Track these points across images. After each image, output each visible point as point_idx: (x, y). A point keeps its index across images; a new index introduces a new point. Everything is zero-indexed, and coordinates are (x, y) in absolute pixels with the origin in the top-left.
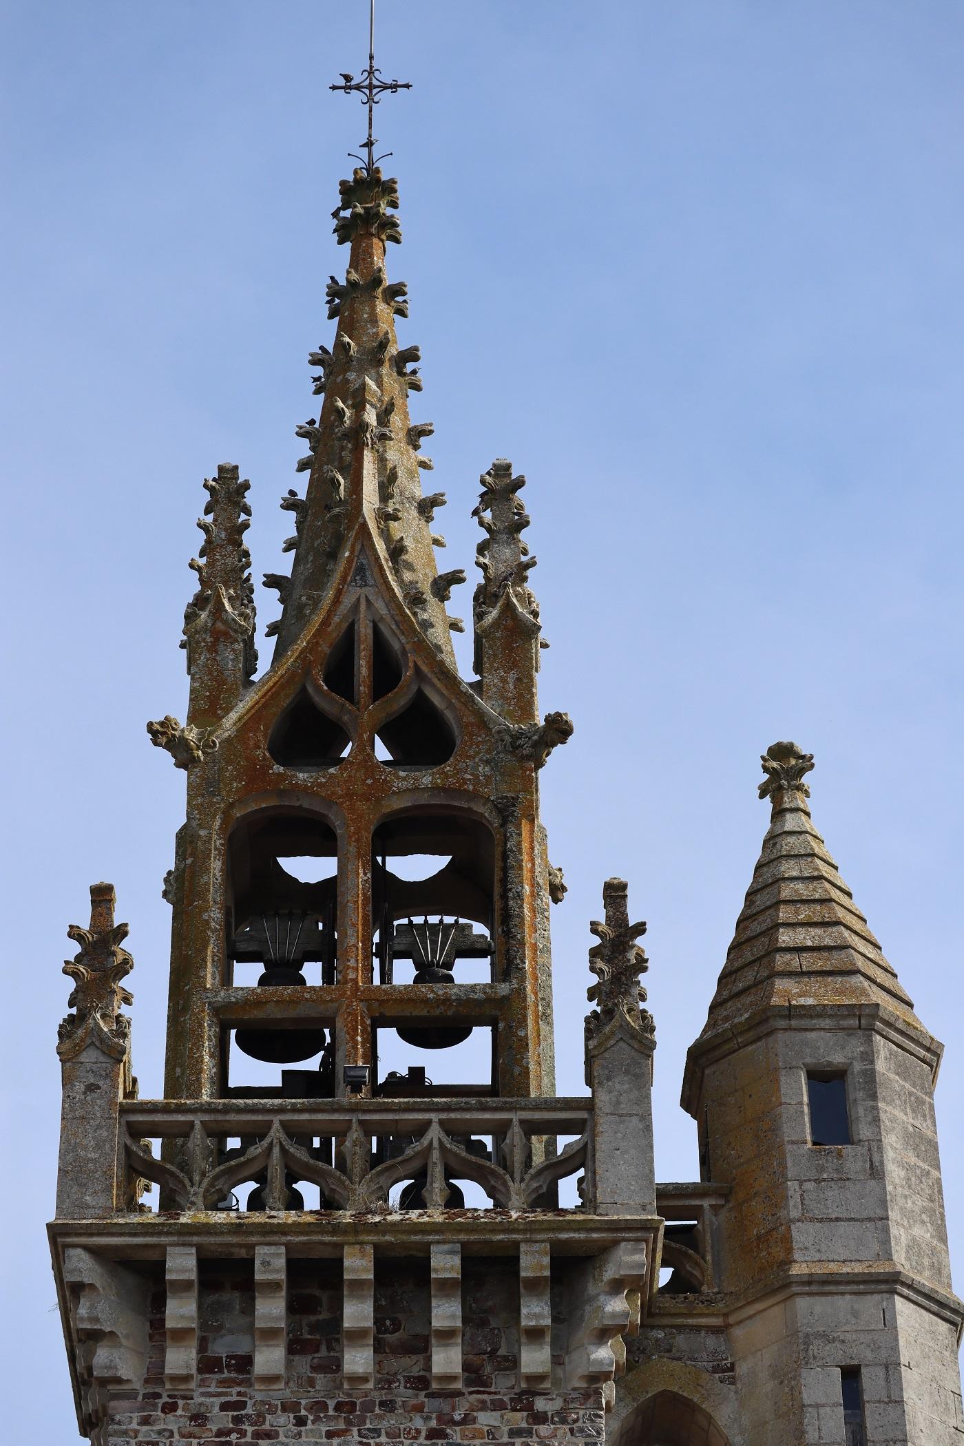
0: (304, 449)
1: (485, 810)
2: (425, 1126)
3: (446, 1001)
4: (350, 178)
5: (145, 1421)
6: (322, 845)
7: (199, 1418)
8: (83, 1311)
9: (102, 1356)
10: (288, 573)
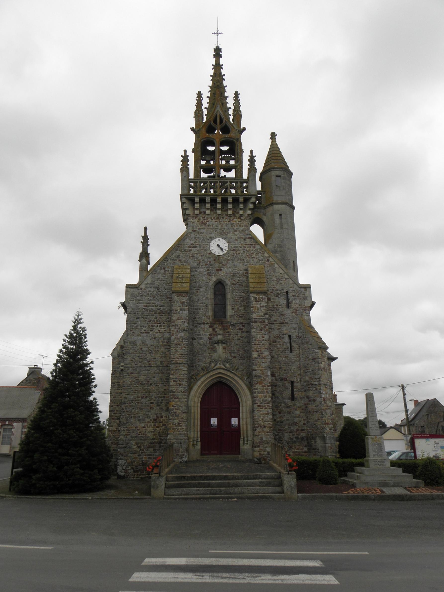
0: (209, 89)
1: (235, 141)
2: (227, 182)
3: (230, 166)
4: (215, 48)
5: (193, 220)
6: (213, 144)
7: (199, 219)
8: (184, 206)
9: (187, 212)
10: (209, 96)
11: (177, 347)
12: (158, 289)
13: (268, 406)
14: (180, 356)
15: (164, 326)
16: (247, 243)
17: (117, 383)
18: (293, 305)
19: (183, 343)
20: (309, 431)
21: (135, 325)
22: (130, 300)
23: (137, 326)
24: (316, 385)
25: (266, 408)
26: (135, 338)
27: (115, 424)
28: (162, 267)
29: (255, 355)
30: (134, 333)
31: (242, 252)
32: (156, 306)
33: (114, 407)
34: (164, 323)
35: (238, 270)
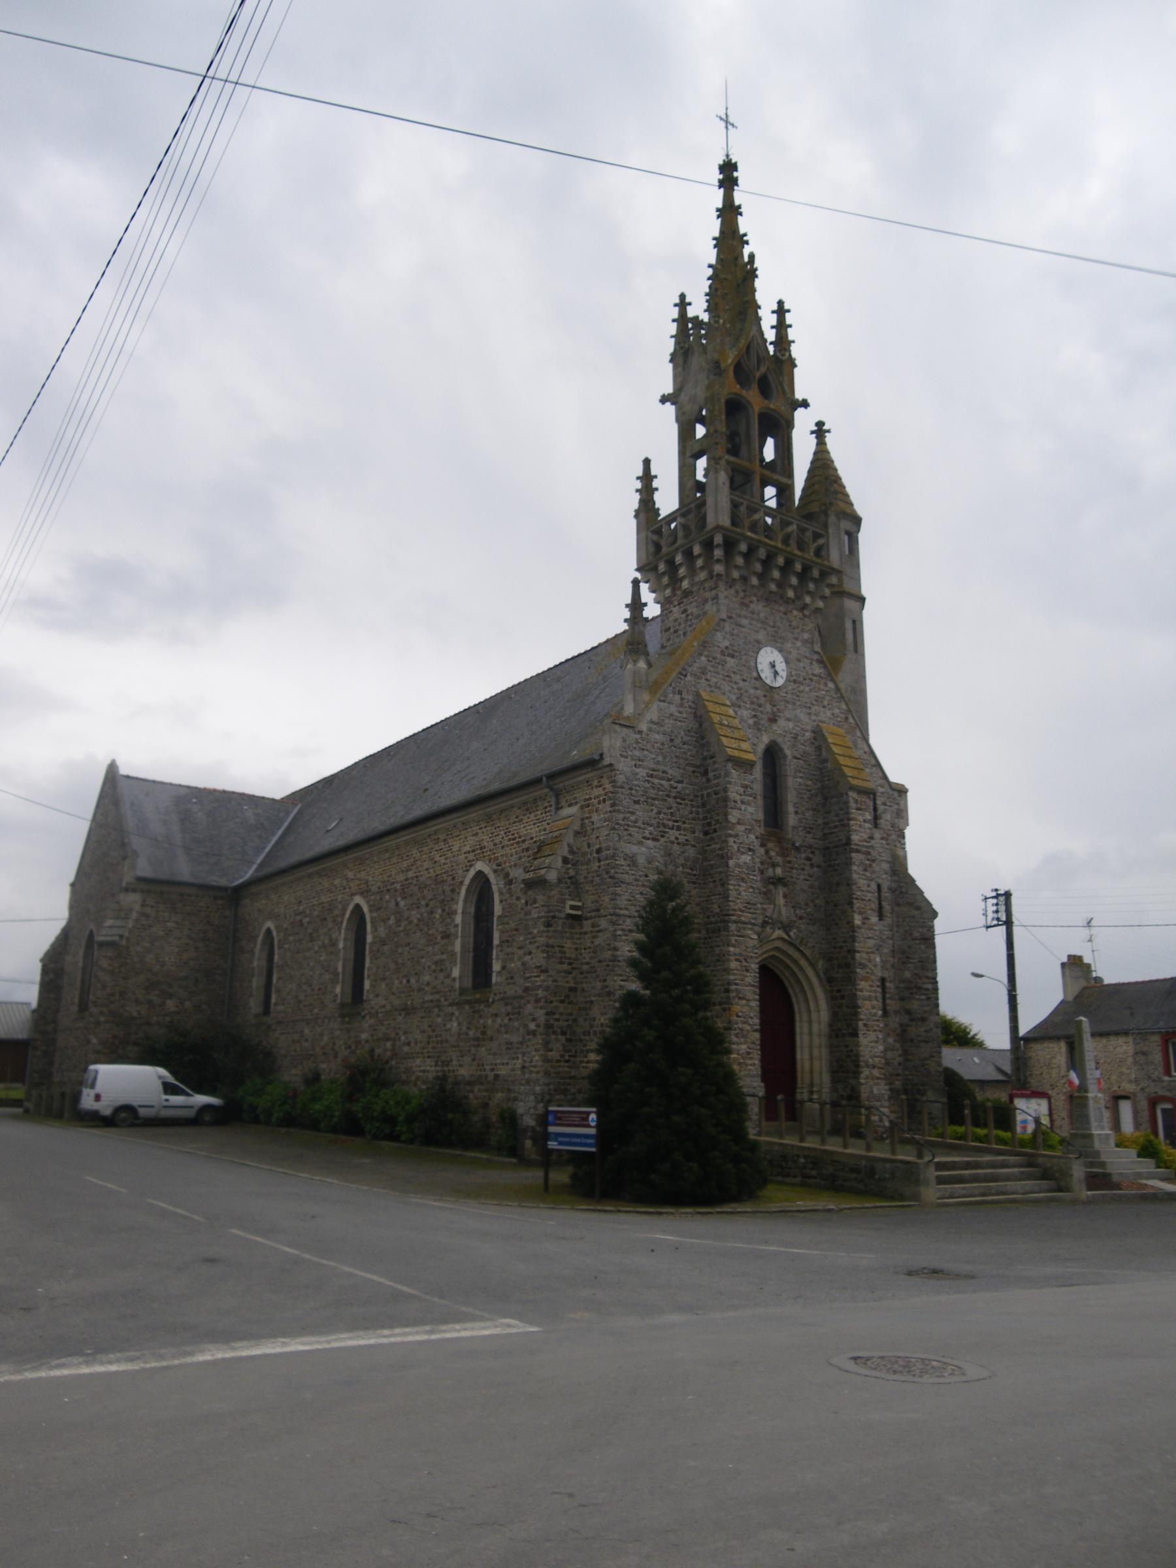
11: (739, 886)
12: (672, 740)
13: (878, 1026)
14: (745, 907)
15: (685, 829)
16: (815, 673)
17: (559, 946)
18: (882, 822)
19: (749, 878)
20: (910, 1077)
21: (633, 818)
22: (622, 756)
23: (636, 821)
24: (927, 989)
25: (875, 1031)
26: (635, 849)
27: (558, 1045)
28: (677, 689)
29: (858, 921)
30: (630, 835)
31: (807, 689)
32: (669, 780)
33: (555, 1004)
34: (684, 823)
35: (802, 729)
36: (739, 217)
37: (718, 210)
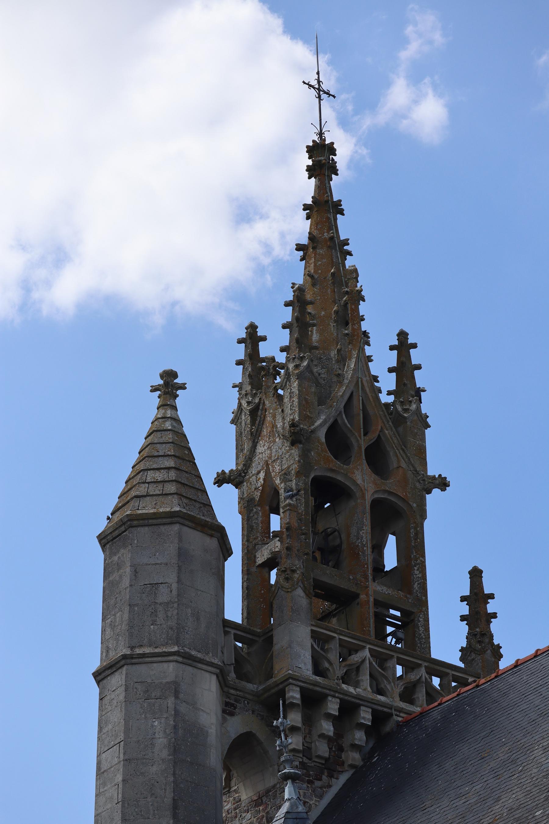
36: (361, 302)
37: (501, 647)
